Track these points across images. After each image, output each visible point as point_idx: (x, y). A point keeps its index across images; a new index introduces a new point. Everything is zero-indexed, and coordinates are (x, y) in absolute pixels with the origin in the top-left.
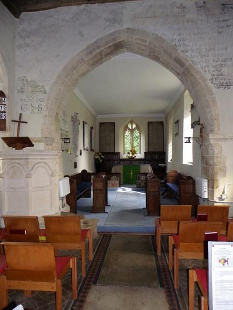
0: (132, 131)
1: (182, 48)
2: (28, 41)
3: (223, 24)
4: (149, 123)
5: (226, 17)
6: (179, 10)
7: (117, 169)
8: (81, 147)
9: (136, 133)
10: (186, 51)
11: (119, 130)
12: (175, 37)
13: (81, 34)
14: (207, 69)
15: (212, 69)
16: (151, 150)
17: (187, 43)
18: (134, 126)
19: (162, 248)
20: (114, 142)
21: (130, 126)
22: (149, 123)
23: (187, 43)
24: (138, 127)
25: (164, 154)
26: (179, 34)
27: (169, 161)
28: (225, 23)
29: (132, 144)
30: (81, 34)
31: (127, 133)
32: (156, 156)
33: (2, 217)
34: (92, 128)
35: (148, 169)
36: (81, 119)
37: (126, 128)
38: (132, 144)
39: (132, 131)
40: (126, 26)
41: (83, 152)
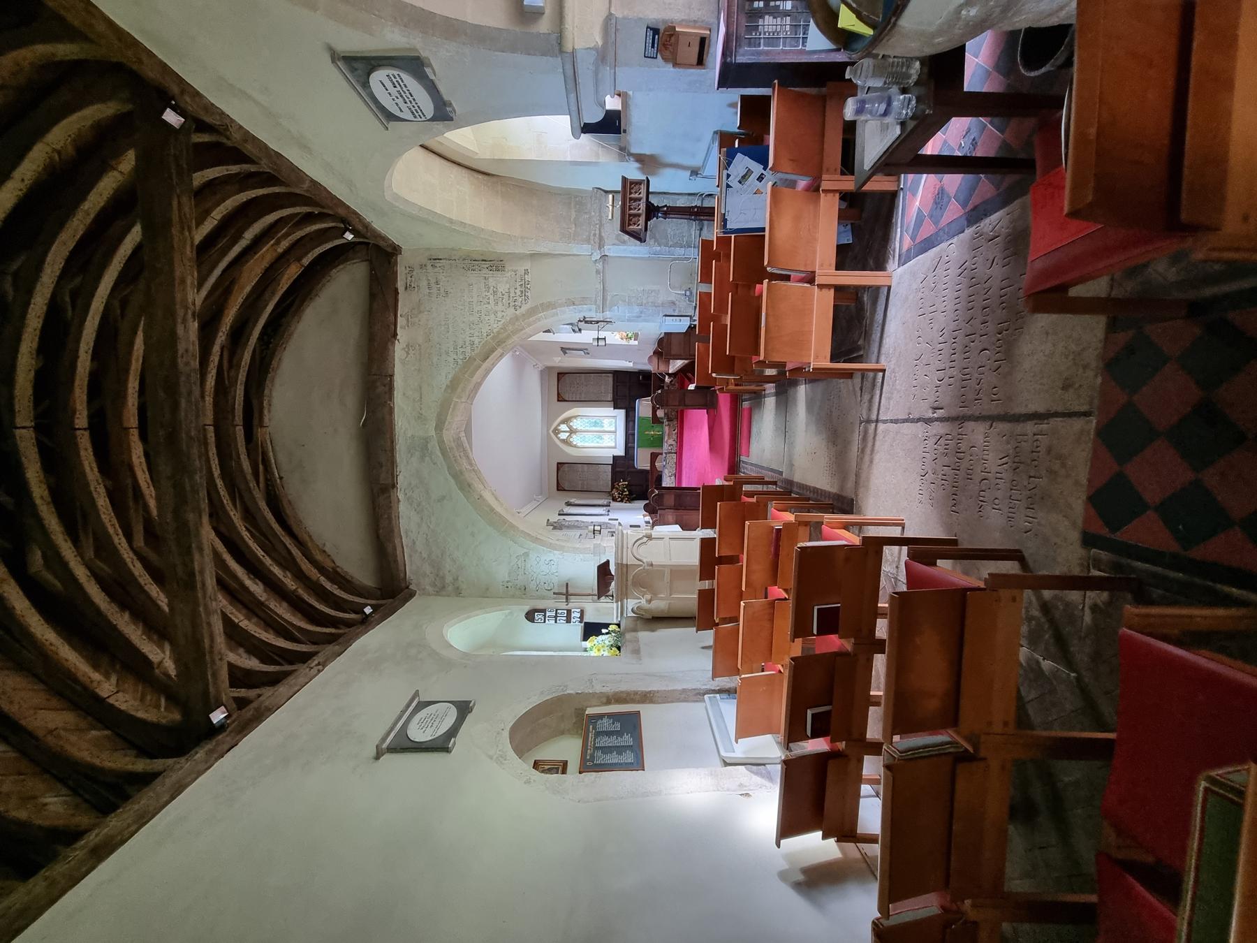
0: (572, 431)
1: (468, 349)
2: (449, 579)
3: (434, 291)
4: (560, 399)
5: (424, 284)
6: (411, 352)
7: (642, 461)
8: (605, 519)
9: (576, 424)
10: (472, 344)
11: (572, 453)
12: (451, 360)
13: (442, 499)
14: (500, 314)
15: (500, 307)
16: (610, 397)
17: (460, 343)
18: (564, 427)
19: (206, 444)
20: (591, 465)
21: (563, 436)
22: (560, 399)
23: (460, 343)
24: (566, 421)
25: (618, 375)
26: (447, 353)
27: (631, 365)
28: (433, 285)
29: (599, 432)
30: (442, 499)
31: (576, 440)
32: (627, 388)
33: (778, 845)
34: (568, 504)
35: (644, 407)
36: (555, 518)
37: (565, 442)
38: (599, 432)
39: (572, 431)
40: (433, 433)
41: (611, 516)
